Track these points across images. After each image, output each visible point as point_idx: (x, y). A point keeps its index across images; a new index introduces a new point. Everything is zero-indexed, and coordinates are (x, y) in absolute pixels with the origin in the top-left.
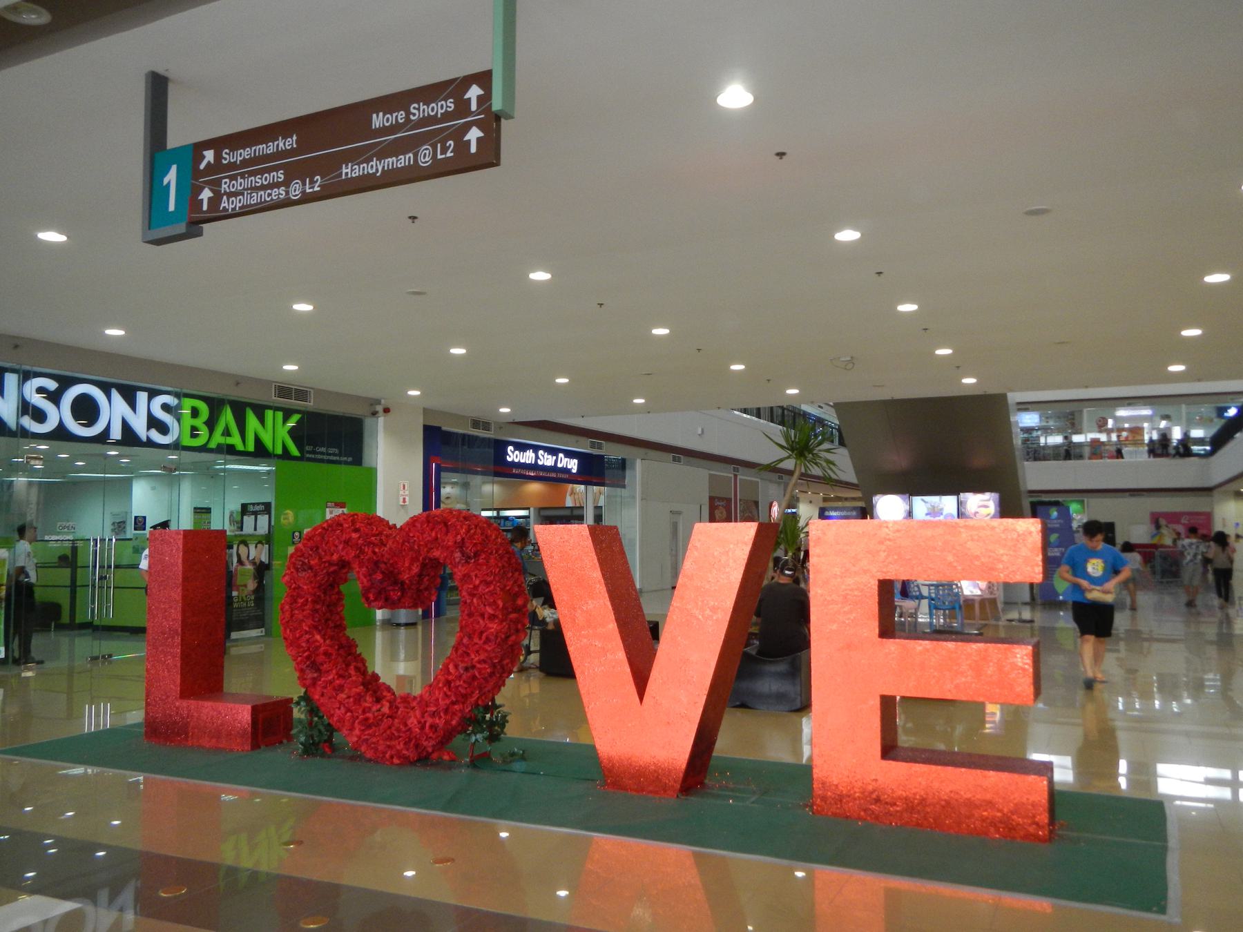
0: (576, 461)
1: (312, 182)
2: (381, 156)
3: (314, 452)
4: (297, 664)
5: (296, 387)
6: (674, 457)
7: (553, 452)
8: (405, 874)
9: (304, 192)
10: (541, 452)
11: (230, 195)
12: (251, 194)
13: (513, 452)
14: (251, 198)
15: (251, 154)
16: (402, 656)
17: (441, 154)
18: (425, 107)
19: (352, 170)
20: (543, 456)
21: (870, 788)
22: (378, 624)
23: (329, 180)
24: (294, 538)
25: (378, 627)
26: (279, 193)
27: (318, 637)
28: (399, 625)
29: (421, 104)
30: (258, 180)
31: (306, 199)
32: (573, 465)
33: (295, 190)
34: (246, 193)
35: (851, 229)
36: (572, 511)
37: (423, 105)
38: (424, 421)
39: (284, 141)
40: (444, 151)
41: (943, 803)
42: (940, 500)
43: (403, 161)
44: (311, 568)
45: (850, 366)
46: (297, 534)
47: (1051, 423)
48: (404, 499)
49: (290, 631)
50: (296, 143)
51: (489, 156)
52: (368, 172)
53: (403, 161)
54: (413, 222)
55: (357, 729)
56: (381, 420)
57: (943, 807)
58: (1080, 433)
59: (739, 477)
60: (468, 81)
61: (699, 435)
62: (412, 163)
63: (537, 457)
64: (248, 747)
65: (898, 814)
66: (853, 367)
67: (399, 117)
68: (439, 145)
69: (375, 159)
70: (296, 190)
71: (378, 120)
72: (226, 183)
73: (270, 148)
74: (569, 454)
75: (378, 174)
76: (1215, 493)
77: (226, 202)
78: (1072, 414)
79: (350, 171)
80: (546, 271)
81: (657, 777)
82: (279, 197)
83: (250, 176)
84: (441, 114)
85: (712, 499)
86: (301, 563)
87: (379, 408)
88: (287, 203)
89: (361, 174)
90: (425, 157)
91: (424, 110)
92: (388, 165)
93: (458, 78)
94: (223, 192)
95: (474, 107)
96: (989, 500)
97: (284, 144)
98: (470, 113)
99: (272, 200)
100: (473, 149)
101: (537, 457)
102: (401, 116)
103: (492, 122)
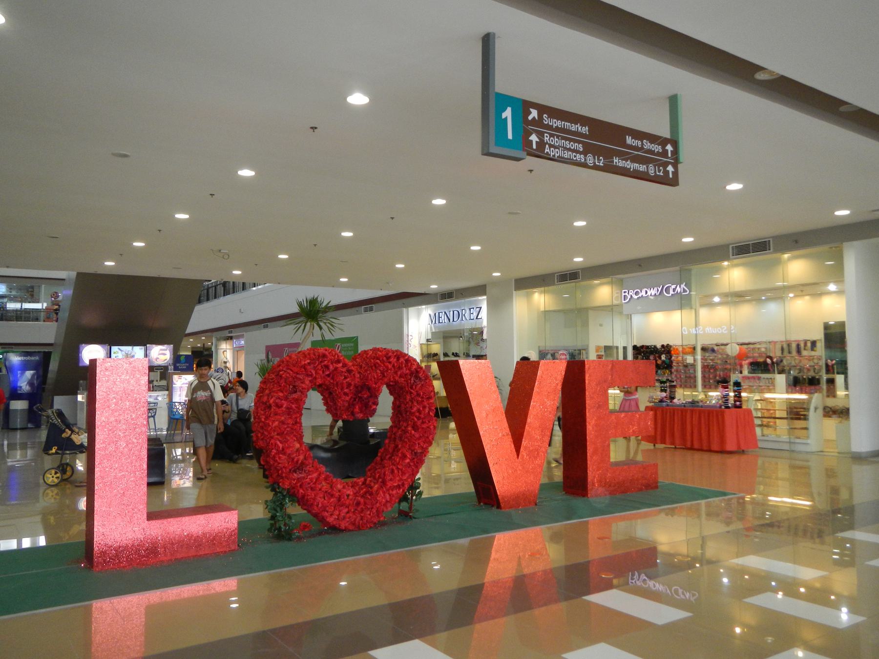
11: (551, 146)
12: (564, 151)
14: (564, 153)
23: (609, 162)
26: (580, 158)
30: (568, 144)
33: (590, 160)
35: (245, 169)
40: (659, 171)
42: (132, 349)
43: (642, 168)
47: (14, 293)
53: (642, 168)
54: (314, 132)
58: (38, 302)
66: (228, 258)
67: (639, 144)
70: (590, 159)
73: (574, 128)
78: (32, 287)
80: (252, 169)
82: (580, 160)
83: (562, 139)
88: (584, 165)
96: (166, 350)
97: (581, 129)
98: (667, 157)
99: (576, 160)
100: (671, 176)
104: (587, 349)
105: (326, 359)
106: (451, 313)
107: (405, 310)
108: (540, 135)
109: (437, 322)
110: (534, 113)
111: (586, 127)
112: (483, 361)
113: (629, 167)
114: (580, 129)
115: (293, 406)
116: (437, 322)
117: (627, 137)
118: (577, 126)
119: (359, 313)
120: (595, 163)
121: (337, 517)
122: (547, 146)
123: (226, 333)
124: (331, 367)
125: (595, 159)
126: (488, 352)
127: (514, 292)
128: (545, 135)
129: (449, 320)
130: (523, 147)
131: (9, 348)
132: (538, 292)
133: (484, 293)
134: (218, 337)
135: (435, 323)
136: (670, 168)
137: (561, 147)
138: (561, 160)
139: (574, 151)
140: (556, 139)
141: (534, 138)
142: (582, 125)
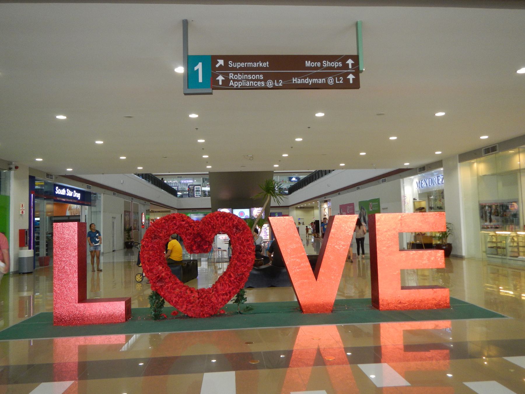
0: (79, 194)
1: (278, 82)
2: (311, 77)
6: (114, 193)
7: (72, 190)
8: (212, 361)
9: (274, 85)
10: (68, 190)
11: (234, 81)
12: (246, 82)
13: (58, 189)
14: (246, 83)
15: (245, 65)
16: (26, 288)
17: (338, 81)
18: (329, 63)
19: (297, 81)
20: (68, 191)
21: (398, 299)
22: (11, 274)
27: (161, 268)
28: (24, 273)
29: (328, 61)
31: (274, 88)
32: (78, 195)
33: (270, 84)
34: (243, 81)
36: (69, 218)
37: (328, 62)
38: (29, 173)
39: (262, 63)
41: (420, 301)
43: (321, 81)
45: (251, 159)
48: (22, 212)
50: (268, 65)
51: (356, 85)
52: (305, 82)
53: (321, 81)
55: (185, 305)
56: (12, 172)
57: (420, 302)
59: (133, 202)
60: (347, 57)
61: (122, 183)
62: (325, 82)
63: (66, 192)
65: (407, 306)
66: (253, 159)
67: (318, 65)
68: (336, 78)
69: (308, 78)
70: (270, 84)
71: (308, 64)
72: (231, 75)
74: (78, 191)
75: (310, 84)
76: (290, 208)
77: (232, 82)
79: (294, 80)
81: (324, 306)
82: (261, 85)
84: (337, 67)
85: (125, 211)
87: (13, 167)
89: (302, 83)
90: (331, 81)
91: (329, 64)
92: (314, 81)
93: (343, 55)
94: (230, 78)
95: (350, 67)
97: (262, 64)
98: (348, 69)
101: (66, 192)
102: (319, 64)
103: (357, 72)
104: (517, 201)
105: (174, 220)
106: (428, 180)
107: (401, 180)
108: (226, 75)
109: (421, 187)
110: (221, 62)
111: (266, 63)
112: (287, 217)
113: (308, 82)
114: (261, 65)
115: (156, 246)
116: (421, 187)
117: (306, 62)
118: (258, 63)
119: (379, 183)
120: (274, 85)
121: (185, 309)
122: (231, 81)
123: (323, 199)
124: (178, 224)
125: (274, 82)
126: (446, 206)
127: (459, 164)
128: (230, 74)
129: (427, 185)
130: (211, 85)
131: (195, 211)
132: (477, 162)
133: (441, 166)
134: (321, 200)
135: (420, 187)
136: (351, 77)
137: (244, 79)
138: (243, 88)
139: (257, 80)
140: (239, 76)
141: (220, 78)
142: (263, 62)
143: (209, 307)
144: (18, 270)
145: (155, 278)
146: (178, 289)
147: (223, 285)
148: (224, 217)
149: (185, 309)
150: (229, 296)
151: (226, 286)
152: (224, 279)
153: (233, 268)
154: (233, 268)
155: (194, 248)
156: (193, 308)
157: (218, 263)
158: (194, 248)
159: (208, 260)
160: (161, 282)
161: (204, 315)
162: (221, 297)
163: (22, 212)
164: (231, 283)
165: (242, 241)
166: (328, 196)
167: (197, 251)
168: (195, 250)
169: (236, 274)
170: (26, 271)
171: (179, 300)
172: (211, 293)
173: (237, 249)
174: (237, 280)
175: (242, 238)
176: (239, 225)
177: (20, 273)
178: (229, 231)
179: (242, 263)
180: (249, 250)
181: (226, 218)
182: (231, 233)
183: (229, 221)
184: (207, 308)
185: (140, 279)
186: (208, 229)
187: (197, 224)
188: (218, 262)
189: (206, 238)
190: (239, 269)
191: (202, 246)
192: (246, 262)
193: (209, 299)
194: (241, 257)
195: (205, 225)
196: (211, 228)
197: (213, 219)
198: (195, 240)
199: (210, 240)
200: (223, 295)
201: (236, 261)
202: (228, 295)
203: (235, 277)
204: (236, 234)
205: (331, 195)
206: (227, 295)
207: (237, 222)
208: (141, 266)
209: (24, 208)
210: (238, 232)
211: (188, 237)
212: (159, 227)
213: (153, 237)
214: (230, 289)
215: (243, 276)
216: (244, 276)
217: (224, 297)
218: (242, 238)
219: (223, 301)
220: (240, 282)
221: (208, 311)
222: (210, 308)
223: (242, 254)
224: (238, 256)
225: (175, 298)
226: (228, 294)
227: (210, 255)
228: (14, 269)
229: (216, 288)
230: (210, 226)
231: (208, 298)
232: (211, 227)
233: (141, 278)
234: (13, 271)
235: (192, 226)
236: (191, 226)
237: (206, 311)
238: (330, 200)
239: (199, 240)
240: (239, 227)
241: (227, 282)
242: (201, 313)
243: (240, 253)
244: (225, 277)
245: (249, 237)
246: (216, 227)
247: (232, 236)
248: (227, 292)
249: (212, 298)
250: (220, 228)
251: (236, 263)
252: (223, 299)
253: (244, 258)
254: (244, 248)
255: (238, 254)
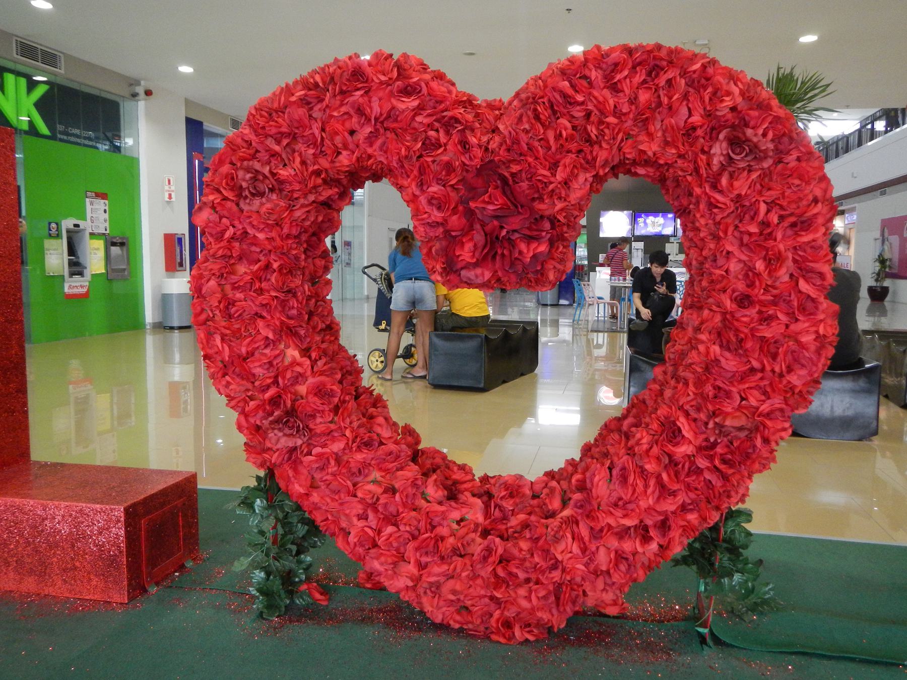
3: (68, 134)
4: (244, 414)
5: (43, 48)
16: (177, 357)
22: (148, 327)
24: (50, 230)
25: (148, 331)
27: (292, 353)
28: (172, 328)
44: (279, 186)
46: (53, 225)
48: (170, 197)
49: (223, 340)
55: (412, 561)
56: (142, 104)
64: (120, 596)
86: (249, 176)
87: (140, 90)
143: (542, 593)
144: (161, 320)
145: (258, 407)
146: (376, 475)
147: (624, 479)
148: (655, 70)
149: (410, 584)
150: (661, 546)
151: (646, 486)
152: (631, 442)
153: (692, 387)
154: (692, 387)
155: (466, 253)
156: (451, 584)
157: (595, 334)
158: (466, 253)
159: (575, 325)
160: (287, 431)
161: (508, 625)
162: (614, 543)
163: (170, 197)
164: (677, 474)
165: (765, 224)
166: (847, 200)
167: (479, 271)
168: (467, 267)
169: (711, 425)
170: (176, 324)
171: (379, 532)
172: (552, 515)
173: (727, 271)
174: (717, 462)
175: (763, 208)
176: (752, 123)
177: (165, 328)
178: (681, 156)
179: (756, 364)
180: (803, 285)
181: (670, 75)
182: (697, 170)
183: (685, 97)
184: (530, 592)
185: (379, 363)
186: (552, 142)
187: (491, 118)
188: (596, 331)
189: (541, 199)
190: (728, 395)
191: (512, 244)
192: (780, 357)
193: (541, 542)
194: (747, 324)
195: (537, 117)
196: (570, 138)
197: (585, 83)
198: (472, 205)
199: (562, 210)
200: (623, 533)
201: (716, 349)
202: (651, 538)
203: (699, 441)
204: (724, 181)
205: (857, 198)
206: (646, 539)
207: (739, 100)
208: (383, 330)
209: (173, 188)
210: (742, 165)
211: (435, 188)
212: (274, 131)
213: (244, 185)
214: (669, 506)
215: (749, 439)
216: (759, 442)
217: (627, 546)
218: (763, 208)
219: (623, 567)
220: (730, 471)
221: (532, 611)
222: (545, 598)
223: (758, 307)
224: (728, 319)
225: (360, 517)
226: (652, 533)
227: (578, 313)
228: (153, 318)
229: (582, 487)
230: (564, 121)
231: (538, 539)
232: (574, 128)
233: (382, 362)
234: (151, 321)
235: (457, 121)
236: (448, 124)
237: (524, 610)
238: (852, 210)
239: (491, 207)
240: (749, 132)
241: (647, 467)
242: (497, 614)
243: (744, 301)
244: (638, 436)
245: (816, 201)
246: (602, 134)
247: (698, 191)
248: (649, 522)
249: (561, 546)
250: (628, 135)
251: (717, 361)
252: (620, 556)
253: (768, 334)
254: (771, 271)
255: (728, 303)
